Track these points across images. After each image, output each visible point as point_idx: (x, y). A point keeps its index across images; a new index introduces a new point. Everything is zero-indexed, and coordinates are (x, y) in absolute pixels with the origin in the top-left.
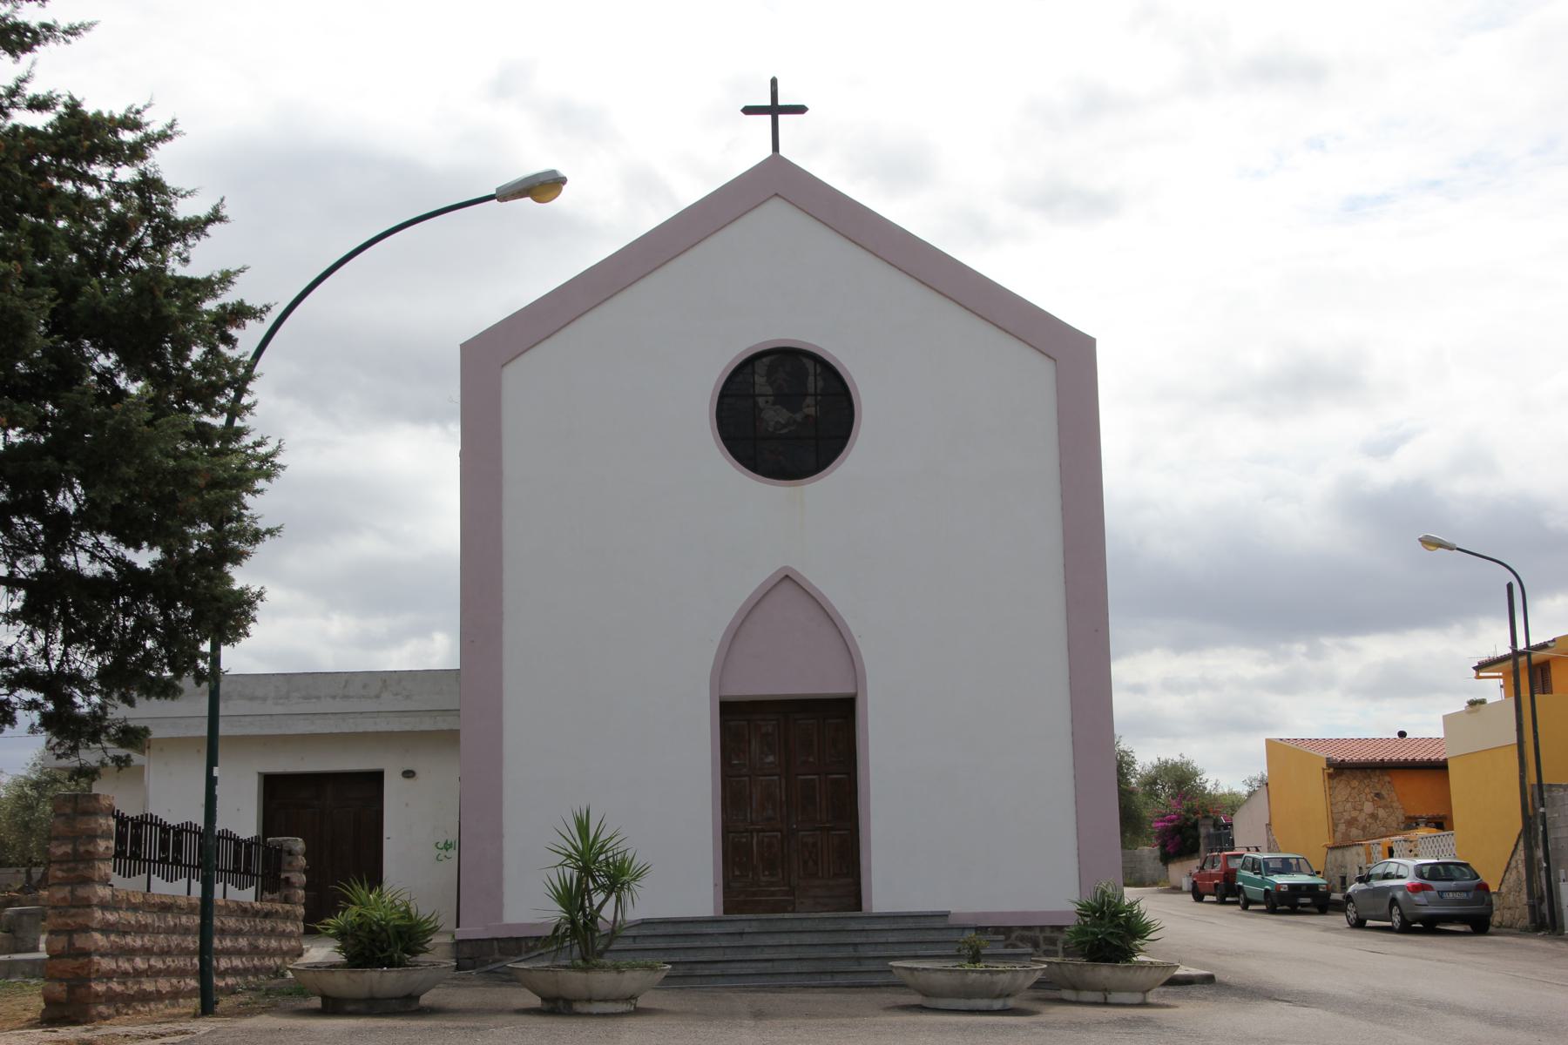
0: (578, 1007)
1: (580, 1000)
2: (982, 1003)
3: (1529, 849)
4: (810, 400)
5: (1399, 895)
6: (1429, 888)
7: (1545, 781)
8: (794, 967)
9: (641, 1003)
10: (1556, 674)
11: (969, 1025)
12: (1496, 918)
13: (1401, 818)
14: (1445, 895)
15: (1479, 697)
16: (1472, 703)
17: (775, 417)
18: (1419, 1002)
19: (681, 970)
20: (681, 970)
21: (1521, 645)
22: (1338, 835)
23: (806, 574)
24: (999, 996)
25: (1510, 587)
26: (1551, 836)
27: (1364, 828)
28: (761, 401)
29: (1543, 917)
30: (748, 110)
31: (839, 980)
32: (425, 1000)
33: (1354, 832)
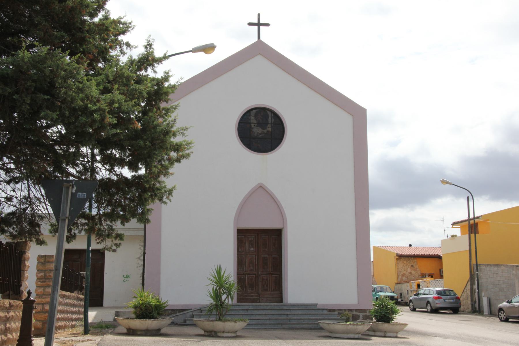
0: (219, 334)
1: (220, 332)
2: (352, 336)
3: (472, 285)
4: (269, 126)
5: (430, 300)
6: (441, 298)
7: (478, 263)
8: (268, 322)
9: (238, 334)
10: (480, 228)
11: (160, 340)
12: (462, 308)
13: (420, 274)
14: (446, 300)
15: (455, 234)
16: (453, 236)
17: (257, 131)
18: (486, 339)
19: (254, 322)
20: (254, 322)
21: (472, 216)
22: (399, 279)
23: (267, 185)
24: (357, 333)
25: (468, 198)
26: (480, 281)
27: (407, 277)
28: (252, 125)
29: (476, 308)
30: (250, 24)
31: (284, 326)
32: (162, 331)
33: (404, 278)
